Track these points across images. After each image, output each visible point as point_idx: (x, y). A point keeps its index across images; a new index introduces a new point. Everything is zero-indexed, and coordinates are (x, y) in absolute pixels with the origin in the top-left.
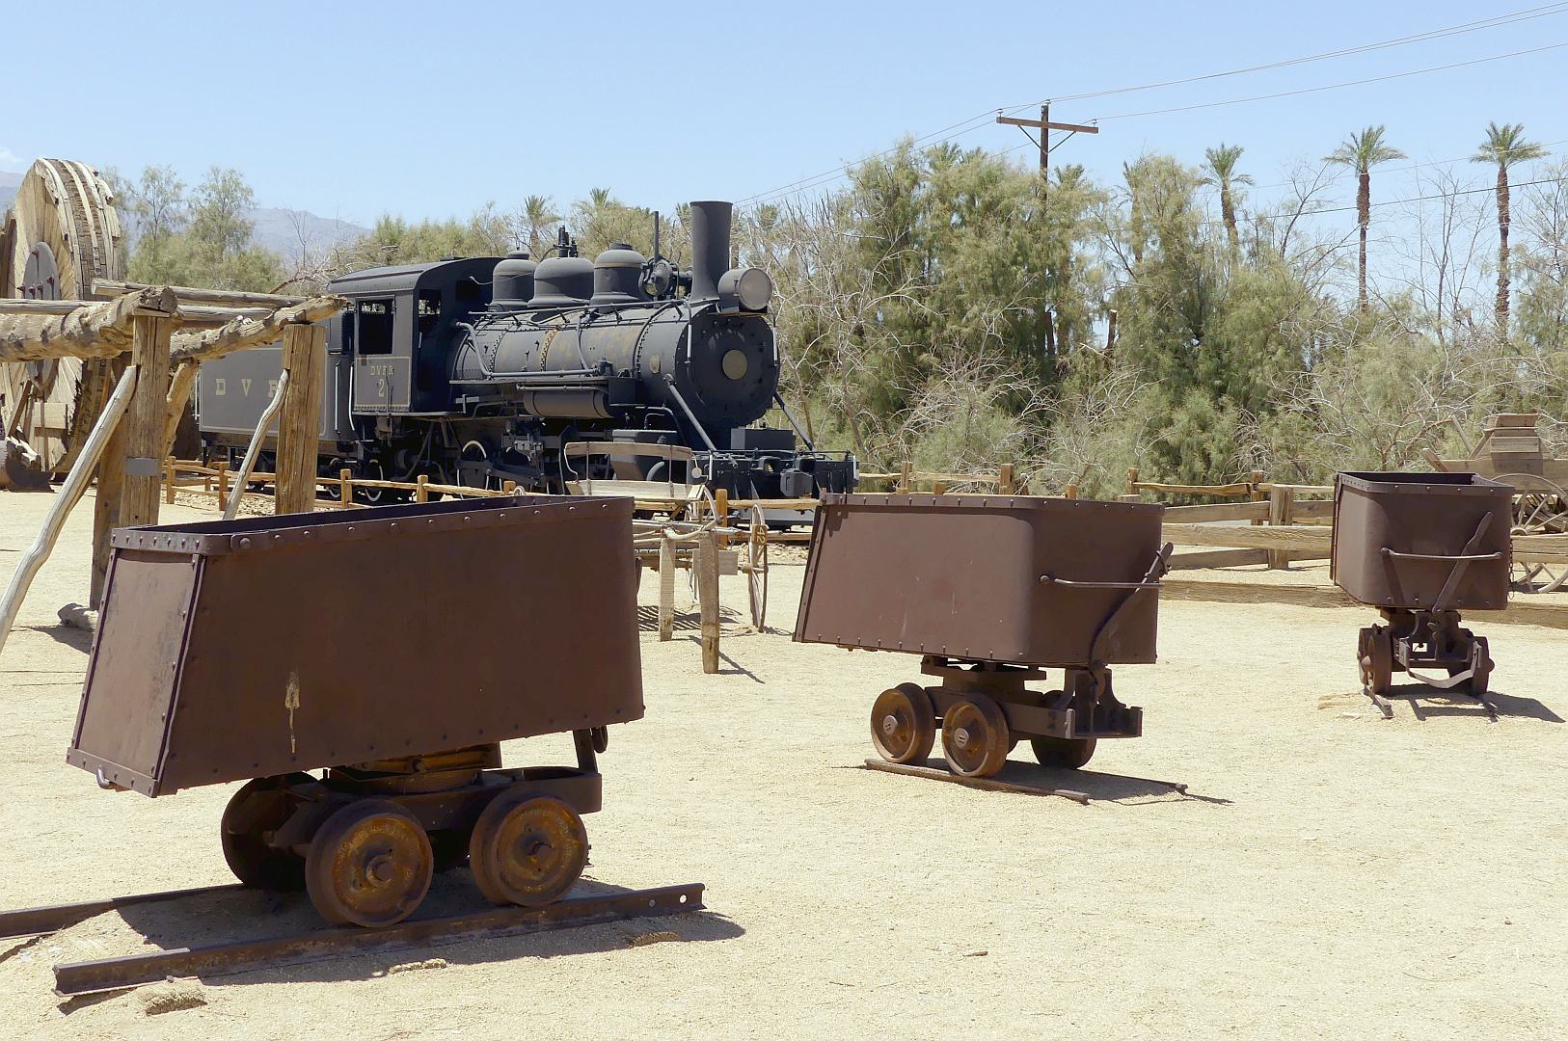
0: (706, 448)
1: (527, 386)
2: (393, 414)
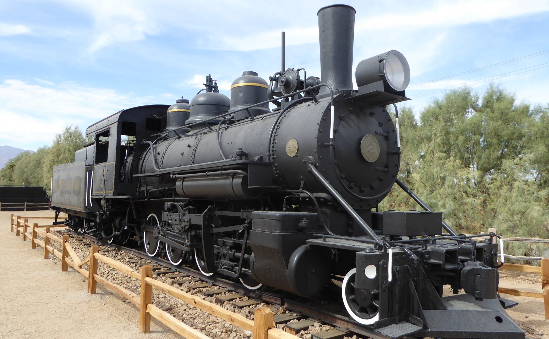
0: (363, 233)
1: (178, 174)
2: (106, 197)
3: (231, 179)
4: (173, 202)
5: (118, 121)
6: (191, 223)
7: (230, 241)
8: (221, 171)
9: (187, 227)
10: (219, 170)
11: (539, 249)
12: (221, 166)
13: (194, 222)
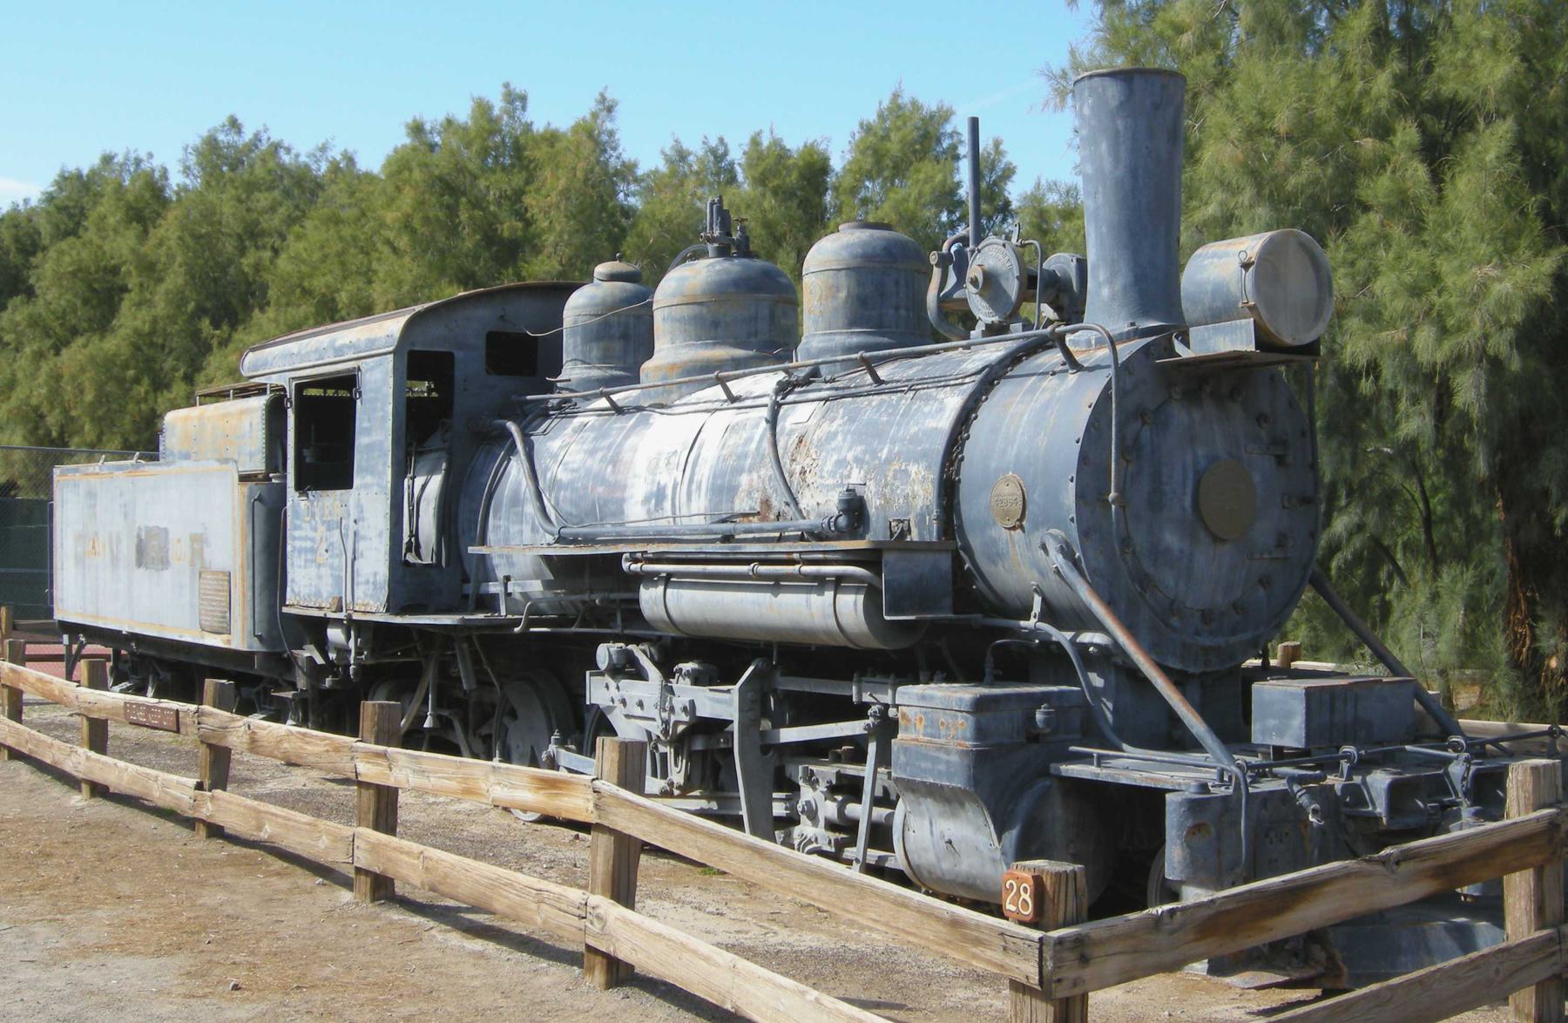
2: (356, 617)
3: (832, 593)
4: (622, 644)
5: (394, 352)
6: (698, 714)
7: (827, 772)
8: (797, 567)
9: (681, 728)
10: (792, 562)
11: (499, 527)
12: (800, 553)
13: (704, 711)
